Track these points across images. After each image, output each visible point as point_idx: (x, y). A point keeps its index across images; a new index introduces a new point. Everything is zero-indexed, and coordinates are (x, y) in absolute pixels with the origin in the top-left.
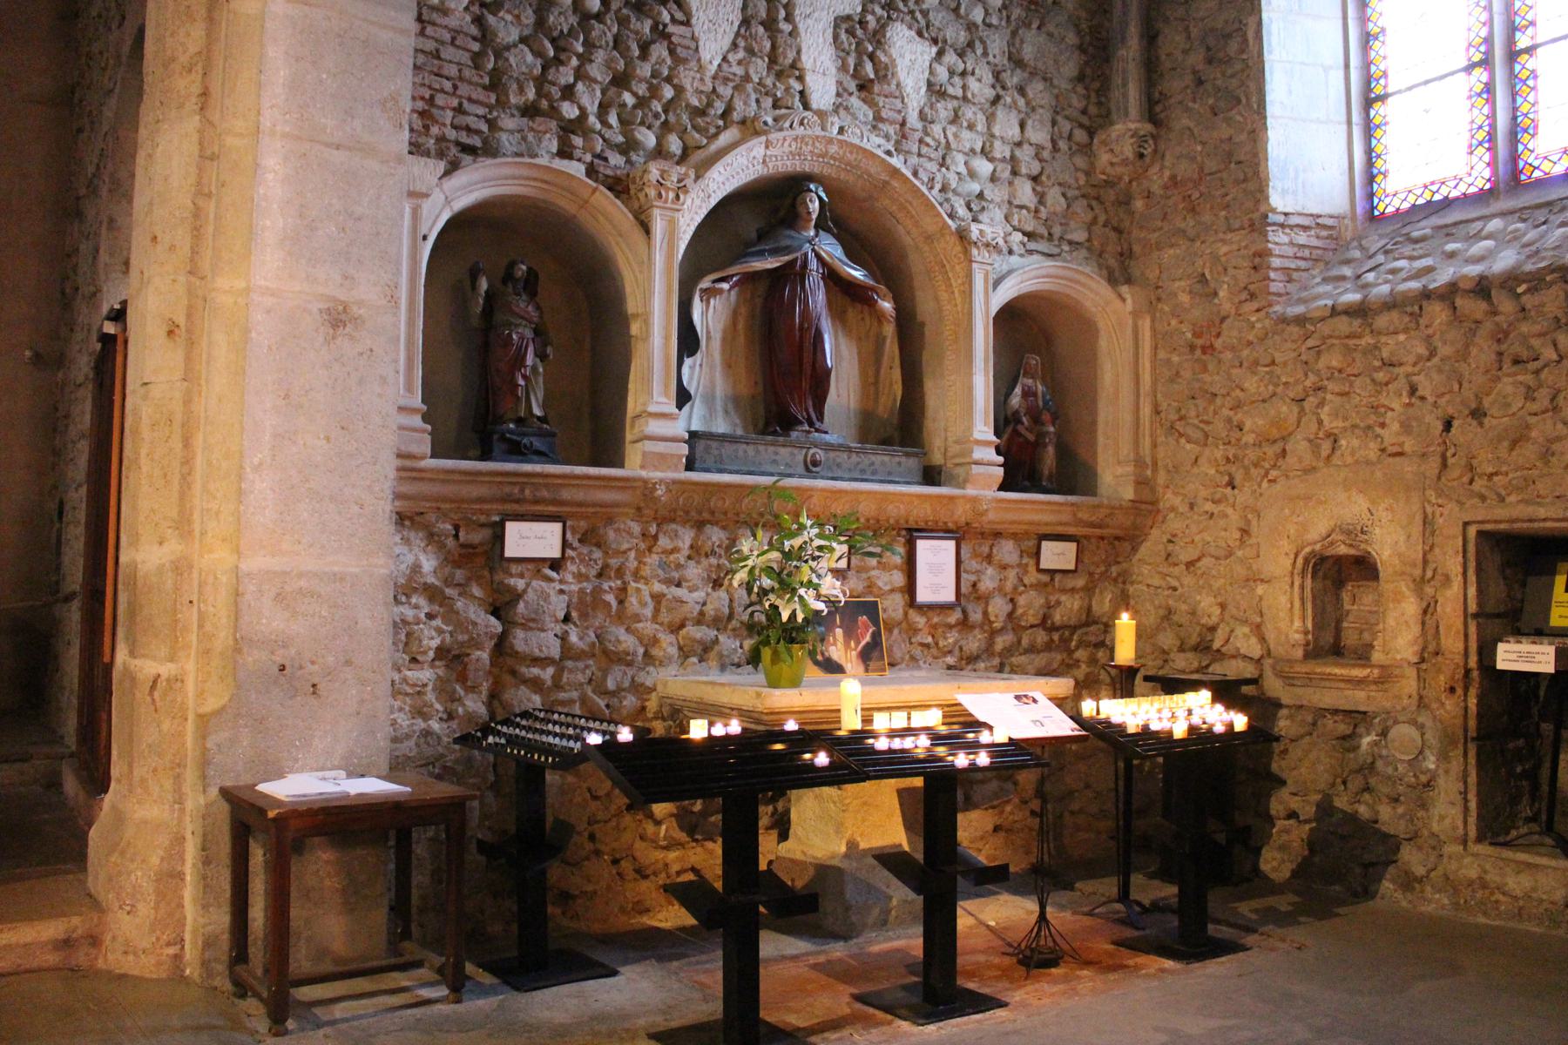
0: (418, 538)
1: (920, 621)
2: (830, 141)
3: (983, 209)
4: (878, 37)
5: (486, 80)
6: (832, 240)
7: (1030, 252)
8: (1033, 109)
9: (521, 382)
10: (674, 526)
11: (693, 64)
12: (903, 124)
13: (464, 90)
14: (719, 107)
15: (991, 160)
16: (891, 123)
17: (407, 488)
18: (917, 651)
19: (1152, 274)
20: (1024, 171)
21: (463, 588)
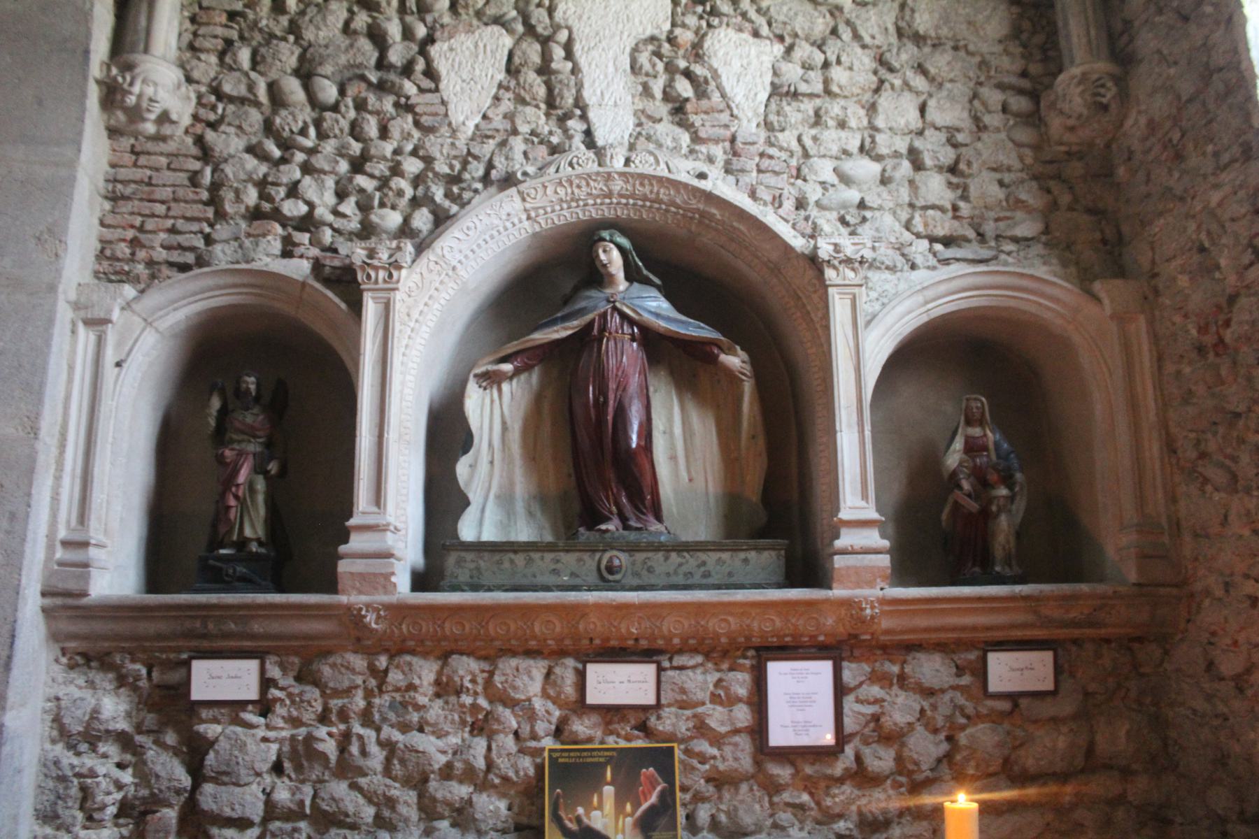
0: (105, 680)
1: (782, 772)
2: (608, 177)
3: (864, 220)
4: (697, 53)
5: (205, 195)
6: (654, 293)
7: (946, 262)
8: (941, 85)
9: (232, 502)
10: (408, 658)
11: (444, 130)
12: (733, 140)
13: (177, 209)
14: (477, 169)
15: (878, 158)
16: (717, 141)
17: (65, 626)
18: (785, 817)
19: (1144, 260)
20: (928, 162)
21: (156, 734)
